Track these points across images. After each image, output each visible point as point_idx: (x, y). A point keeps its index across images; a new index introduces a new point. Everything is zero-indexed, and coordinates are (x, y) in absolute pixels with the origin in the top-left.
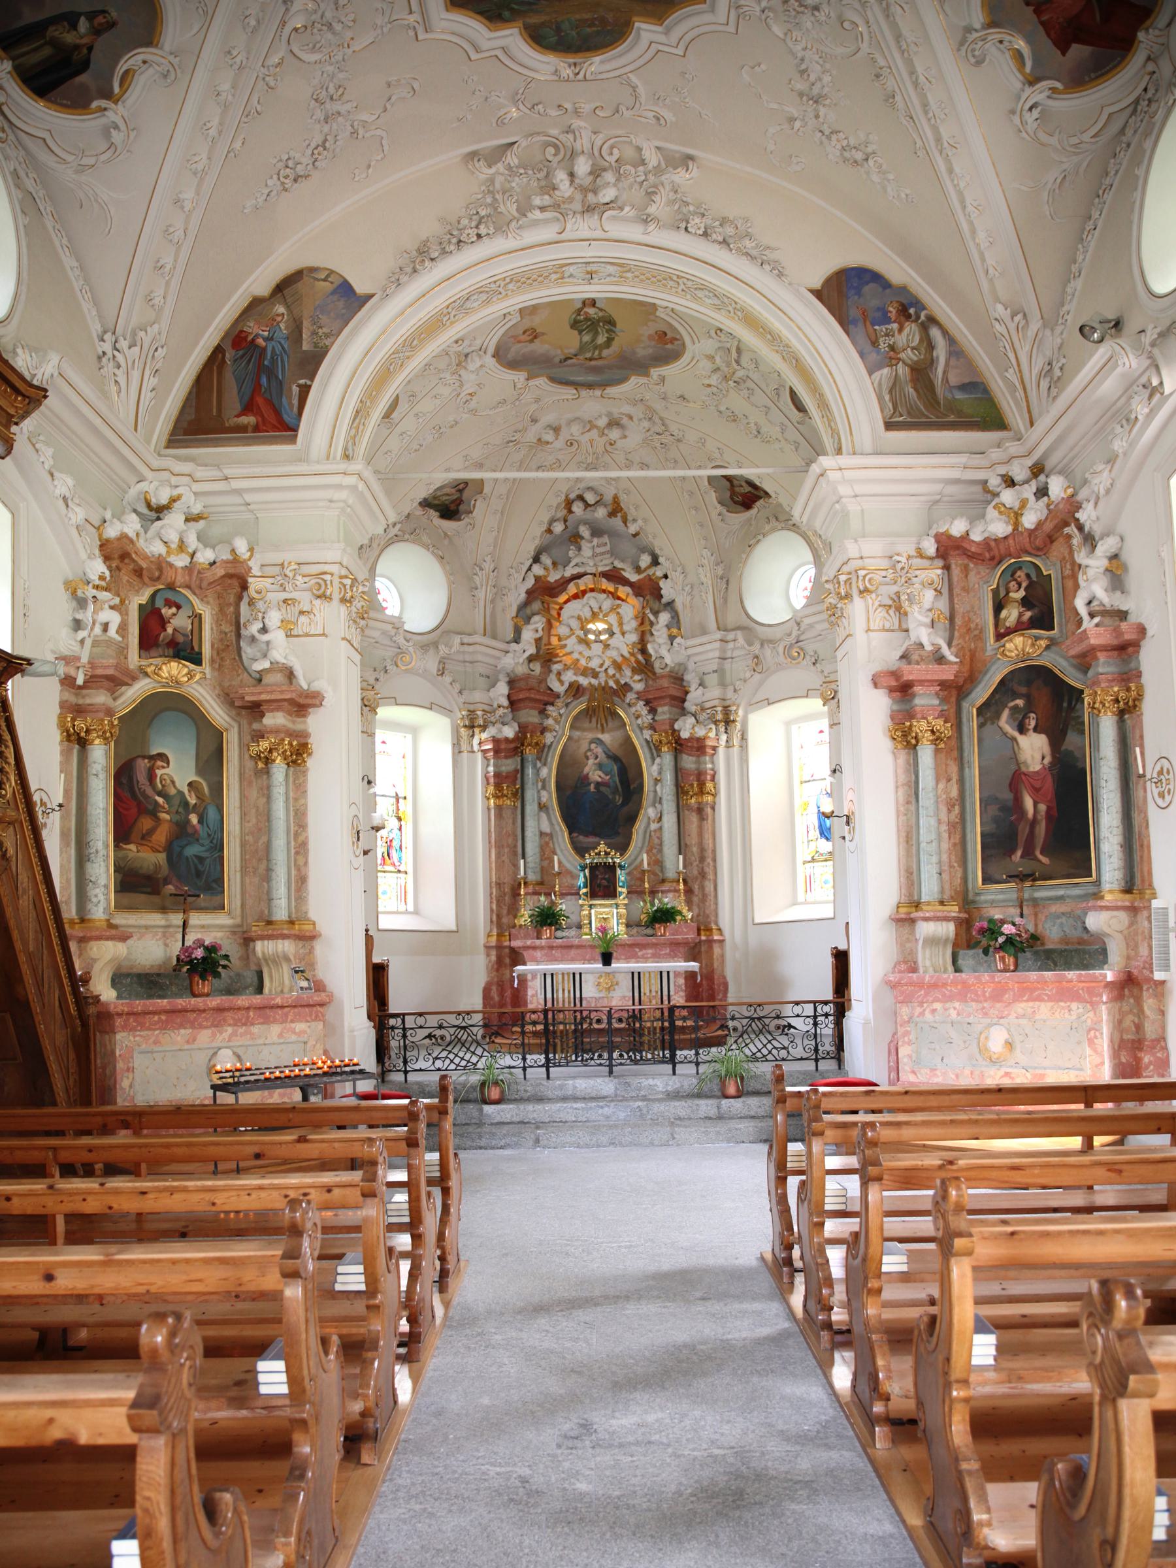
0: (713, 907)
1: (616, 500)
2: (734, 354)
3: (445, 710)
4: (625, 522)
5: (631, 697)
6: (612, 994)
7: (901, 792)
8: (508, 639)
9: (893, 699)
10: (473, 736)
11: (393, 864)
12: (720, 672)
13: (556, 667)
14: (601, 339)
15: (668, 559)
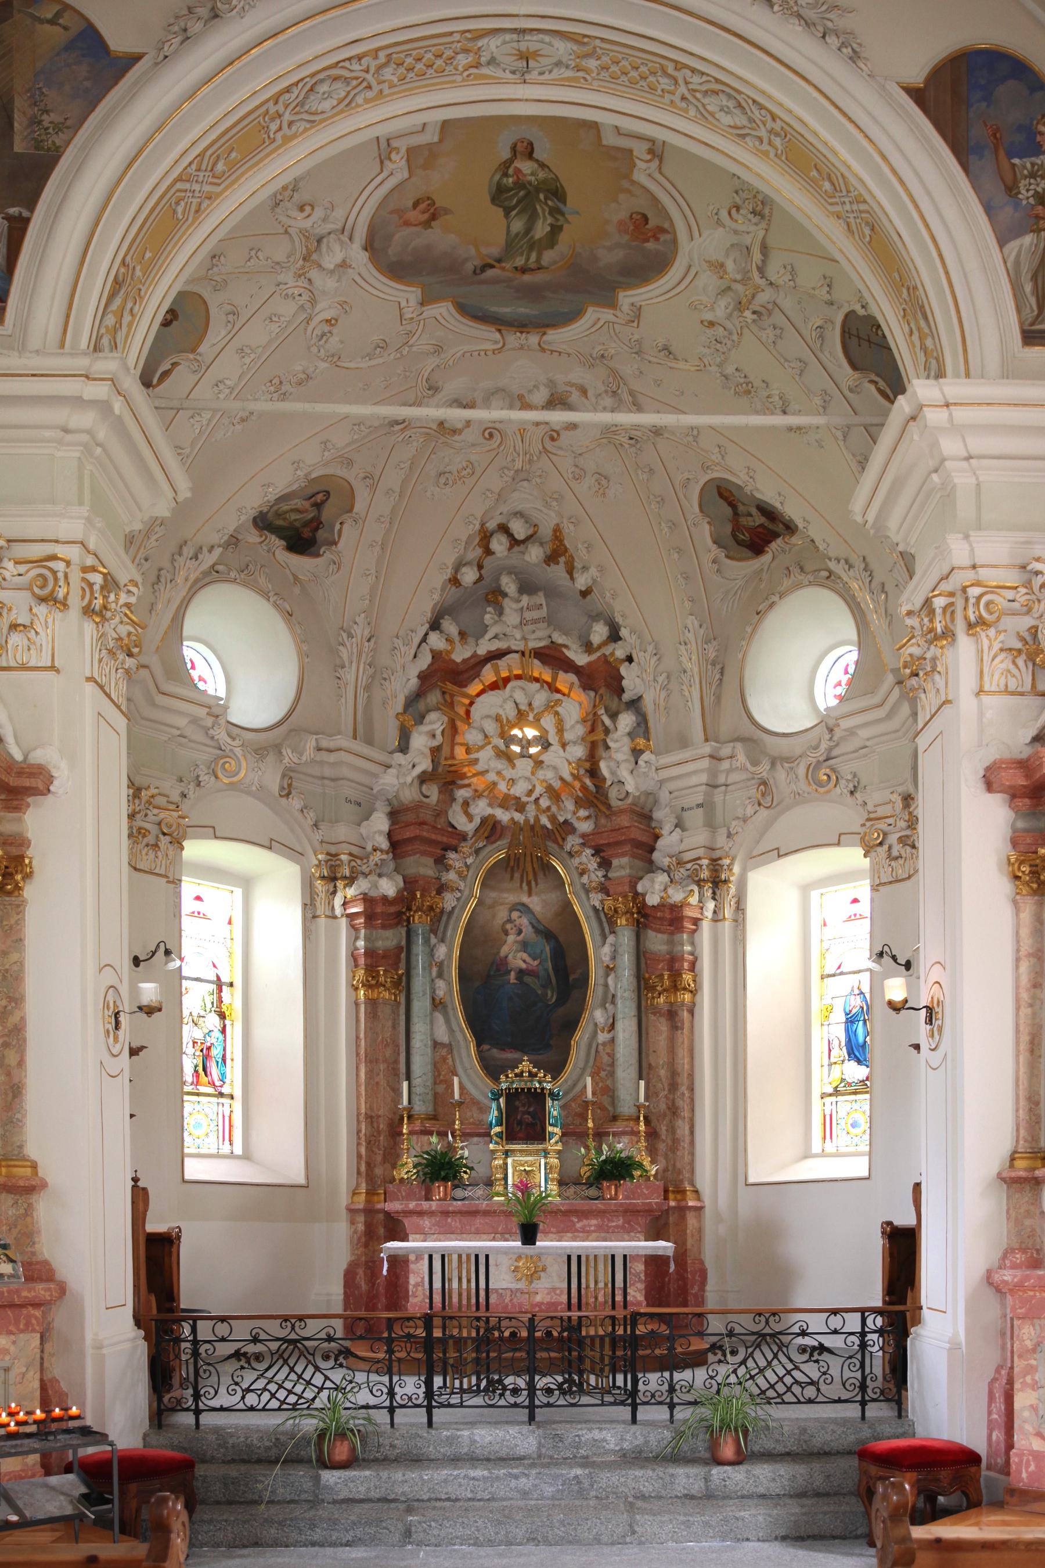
0: (687, 1158)
1: (557, 533)
2: (757, 256)
3: (292, 852)
4: (570, 571)
5: (572, 842)
6: (537, 1285)
7: (1024, 967)
8: (391, 748)
9: (1016, 810)
10: (334, 893)
11: (212, 1084)
12: (707, 806)
13: (462, 794)
14: (541, 230)
15: (633, 631)
